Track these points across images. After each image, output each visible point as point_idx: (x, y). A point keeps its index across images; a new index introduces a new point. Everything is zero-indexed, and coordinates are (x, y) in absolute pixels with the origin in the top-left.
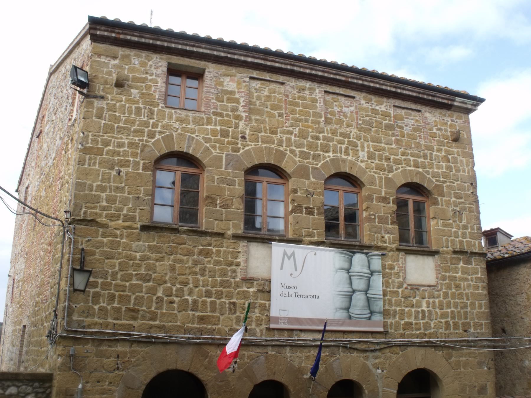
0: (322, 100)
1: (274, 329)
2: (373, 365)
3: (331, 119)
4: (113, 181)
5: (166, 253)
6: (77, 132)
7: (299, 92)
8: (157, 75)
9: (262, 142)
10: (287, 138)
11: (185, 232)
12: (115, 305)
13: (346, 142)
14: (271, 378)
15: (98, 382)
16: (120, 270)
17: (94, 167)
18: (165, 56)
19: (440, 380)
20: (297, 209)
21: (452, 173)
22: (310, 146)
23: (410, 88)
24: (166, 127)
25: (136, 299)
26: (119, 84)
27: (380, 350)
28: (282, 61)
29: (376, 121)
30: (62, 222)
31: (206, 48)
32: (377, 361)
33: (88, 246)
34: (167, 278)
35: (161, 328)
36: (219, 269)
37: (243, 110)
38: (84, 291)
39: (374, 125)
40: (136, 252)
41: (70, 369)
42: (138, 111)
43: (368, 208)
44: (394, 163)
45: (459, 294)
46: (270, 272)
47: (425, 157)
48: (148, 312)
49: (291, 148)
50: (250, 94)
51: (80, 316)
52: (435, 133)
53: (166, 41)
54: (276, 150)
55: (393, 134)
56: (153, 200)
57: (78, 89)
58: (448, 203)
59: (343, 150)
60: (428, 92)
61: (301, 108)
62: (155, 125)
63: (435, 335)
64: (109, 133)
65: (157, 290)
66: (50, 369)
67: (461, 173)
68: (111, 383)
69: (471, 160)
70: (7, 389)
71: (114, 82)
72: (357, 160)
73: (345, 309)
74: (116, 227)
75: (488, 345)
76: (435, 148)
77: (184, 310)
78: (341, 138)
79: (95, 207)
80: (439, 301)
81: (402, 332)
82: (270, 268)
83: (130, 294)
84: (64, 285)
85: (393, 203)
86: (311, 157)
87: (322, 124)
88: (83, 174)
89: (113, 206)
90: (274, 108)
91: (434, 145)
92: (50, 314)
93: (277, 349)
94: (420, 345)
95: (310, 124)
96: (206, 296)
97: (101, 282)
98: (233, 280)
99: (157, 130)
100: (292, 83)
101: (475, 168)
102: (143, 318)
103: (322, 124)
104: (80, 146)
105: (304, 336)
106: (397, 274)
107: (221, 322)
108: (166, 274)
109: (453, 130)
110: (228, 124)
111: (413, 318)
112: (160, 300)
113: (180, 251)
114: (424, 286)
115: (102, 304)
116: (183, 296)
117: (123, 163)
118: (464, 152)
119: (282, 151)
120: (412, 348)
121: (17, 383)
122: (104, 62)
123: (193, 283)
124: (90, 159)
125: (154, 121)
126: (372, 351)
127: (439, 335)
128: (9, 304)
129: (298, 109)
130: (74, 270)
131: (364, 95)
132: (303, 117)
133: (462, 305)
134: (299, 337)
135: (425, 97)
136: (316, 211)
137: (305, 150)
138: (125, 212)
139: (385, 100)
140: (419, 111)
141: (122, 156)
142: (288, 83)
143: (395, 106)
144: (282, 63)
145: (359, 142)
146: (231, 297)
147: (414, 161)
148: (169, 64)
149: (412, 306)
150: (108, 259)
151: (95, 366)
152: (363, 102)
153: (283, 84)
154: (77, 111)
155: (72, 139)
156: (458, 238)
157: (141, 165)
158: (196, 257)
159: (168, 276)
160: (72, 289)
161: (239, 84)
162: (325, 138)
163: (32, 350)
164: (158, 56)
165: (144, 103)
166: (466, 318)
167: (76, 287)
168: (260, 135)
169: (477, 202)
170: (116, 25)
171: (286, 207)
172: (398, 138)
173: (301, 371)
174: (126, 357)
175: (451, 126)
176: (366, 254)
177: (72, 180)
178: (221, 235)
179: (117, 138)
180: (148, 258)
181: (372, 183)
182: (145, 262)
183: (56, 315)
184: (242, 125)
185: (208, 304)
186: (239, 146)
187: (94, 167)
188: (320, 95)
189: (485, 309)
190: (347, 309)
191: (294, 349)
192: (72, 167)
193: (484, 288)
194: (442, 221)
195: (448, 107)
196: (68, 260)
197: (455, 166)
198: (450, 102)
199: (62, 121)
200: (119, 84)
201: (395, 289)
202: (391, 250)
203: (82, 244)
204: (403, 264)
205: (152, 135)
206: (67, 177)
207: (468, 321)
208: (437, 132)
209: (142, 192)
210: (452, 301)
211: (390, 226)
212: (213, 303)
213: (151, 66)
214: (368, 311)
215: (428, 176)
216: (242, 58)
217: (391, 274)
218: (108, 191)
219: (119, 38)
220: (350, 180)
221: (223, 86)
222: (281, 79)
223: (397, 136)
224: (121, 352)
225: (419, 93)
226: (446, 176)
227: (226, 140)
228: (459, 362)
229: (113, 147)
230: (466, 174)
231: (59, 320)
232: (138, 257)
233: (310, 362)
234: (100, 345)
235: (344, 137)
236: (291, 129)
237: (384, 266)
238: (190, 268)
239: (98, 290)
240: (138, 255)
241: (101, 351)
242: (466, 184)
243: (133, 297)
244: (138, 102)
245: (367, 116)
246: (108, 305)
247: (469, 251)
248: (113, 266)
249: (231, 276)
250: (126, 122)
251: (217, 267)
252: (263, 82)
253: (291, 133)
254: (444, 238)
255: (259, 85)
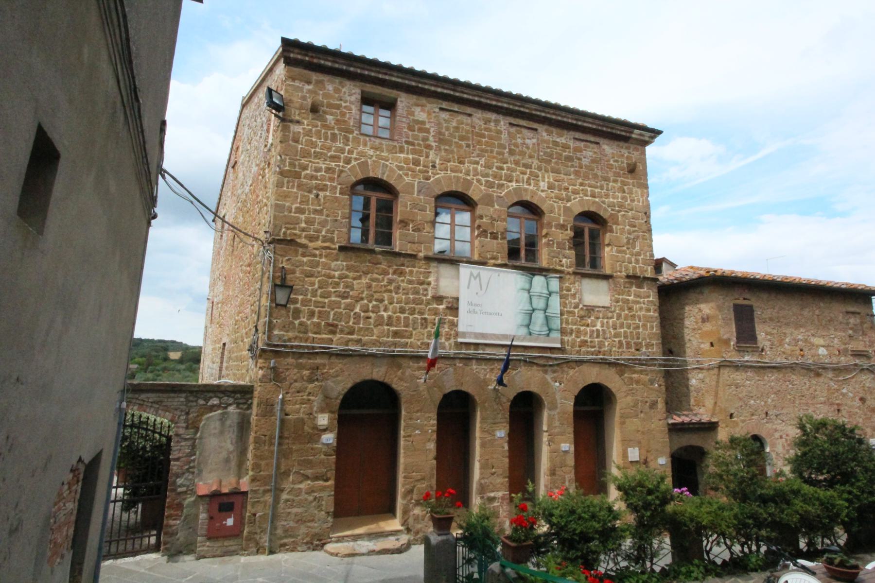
1: (461, 343)
6: (275, 158)
8: (351, 103)
12: (315, 320)
14: (458, 388)
16: (320, 288)
18: (358, 84)
20: (484, 233)
23: (590, 120)
24: (362, 154)
25: (334, 314)
26: (314, 109)
31: (398, 77)
35: (359, 341)
38: (285, 306)
41: (271, 381)
43: (547, 234)
46: (458, 291)
50: (439, 124)
51: (281, 330)
52: (612, 165)
54: (464, 179)
56: (350, 223)
62: (350, 152)
79: (294, 229)
81: (577, 349)
84: (265, 302)
87: (506, 155)
90: (462, 138)
91: (610, 175)
93: (464, 361)
98: (424, 298)
100: (479, 116)
101: (649, 199)
102: (342, 331)
103: (506, 155)
106: (574, 296)
114: (599, 307)
115: (302, 319)
128: (209, 325)
131: (545, 127)
135: (605, 129)
137: (490, 179)
138: (323, 233)
139: (565, 132)
140: (598, 143)
148: (363, 92)
149: (588, 325)
150: (308, 277)
152: (545, 134)
153: (470, 115)
155: (269, 164)
161: (429, 114)
164: (352, 83)
165: (339, 129)
167: (278, 302)
171: (472, 232)
175: (627, 158)
176: (545, 276)
177: (272, 201)
178: (413, 257)
180: (347, 277)
183: (257, 330)
186: (430, 174)
195: (626, 139)
196: (269, 278)
199: (257, 148)
200: (314, 109)
205: (348, 161)
206: (265, 200)
212: (406, 318)
213: (345, 93)
214: (547, 329)
216: (433, 88)
220: (532, 209)
222: (469, 110)
225: (599, 125)
232: (337, 276)
234: (300, 358)
235: (527, 168)
236: (477, 159)
237: (561, 289)
238: (385, 286)
240: (337, 274)
243: (332, 313)
244: (333, 128)
245: (548, 147)
246: (308, 319)
248: (313, 284)
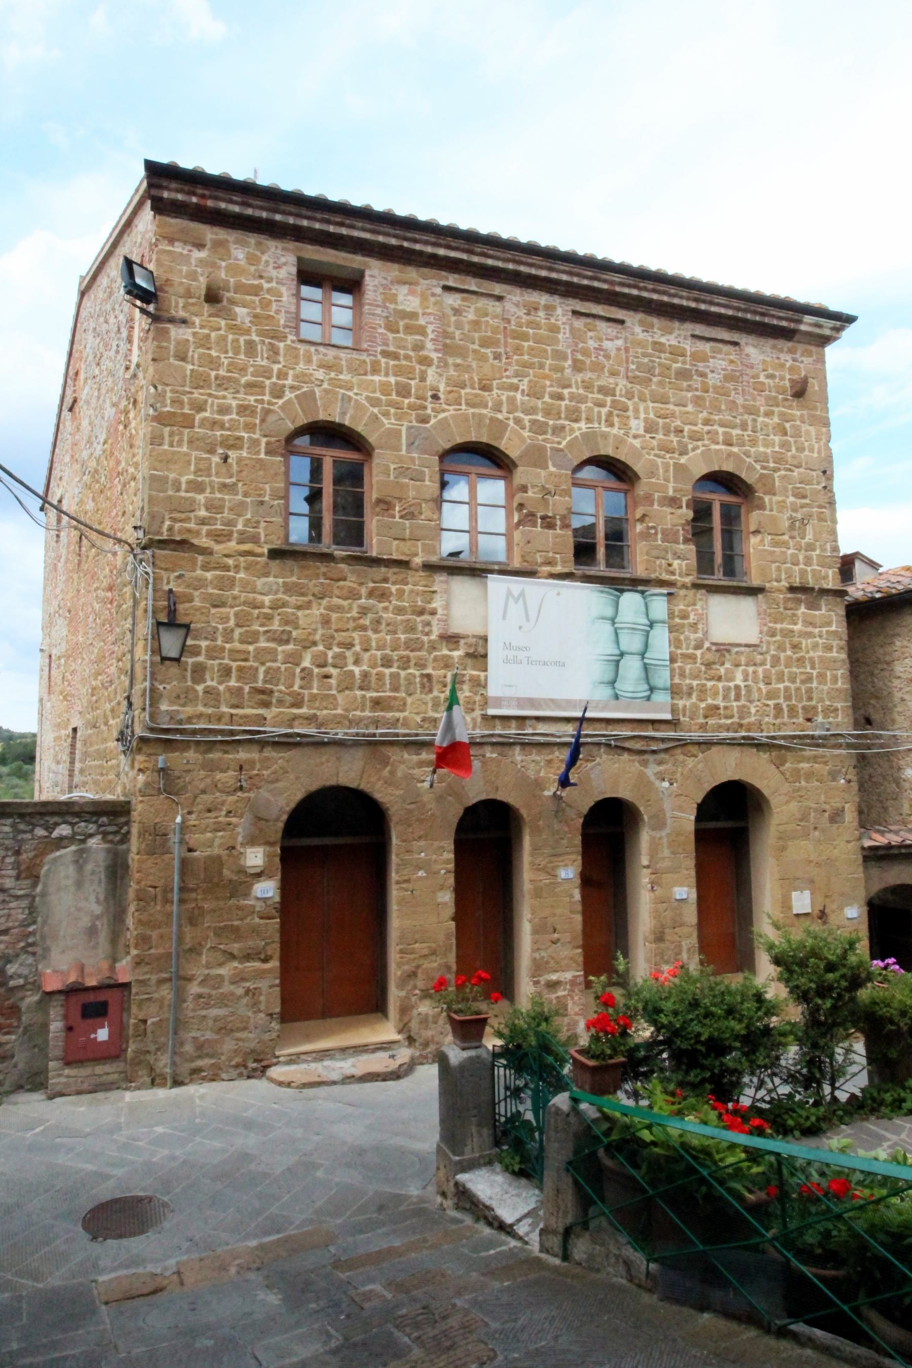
0: (567, 327)
1: (494, 717)
2: (655, 774)
3: (583, 362)
4: (217, 474)
5: (314, 595)
7: (528, 314)
9: (467, 404)
10: (508, 398)
11: (344, 560)
12: (233, 683)
13: (609, 404)
15: (209, 811)
17: (179, 449)
18: (292, 245)
19: (766, 801)
20: (529, 518)
21: (789, 454)
22: (547, 413)
24: (302, 378)
25: (267, 672)
26: (212, 297)
27: (666, 750)
28: (498, 254)
29: (660, 364)
30: (129, 545)
31: (364, 229)
32: (661, 768)
33: (179, 586)
34: (317, 637)
35: (311, 719)
36: (403, 621)
37: (433, 347)
38: (177, 660)
39: (657, 372)
40: (262, 594)
41: (160, 793)
42: (251, 347)
43: (644, 516)
44: (691, 438)
45: (798, 660)
47: (744, 426)
48: (288, 694)
49: (516, 414)
50: (442, 317)
51: (172, 703)
52: (762, 383)
53: (290, 214)
55: (689, 386)
57: (138, 303)
58: (782, 506)
59: (604, 418)
60: (754, 307)
61: (531, 343)
62: (282, 375)
63: (759, 726)
64: (202, 387)
65: (301, 656)
66: (124, 795)
67: (806, 453)
68: (230, 812)
69: (824, 430)
70: (54, 829)
71: (203, 292)
72: (626, 434)
73: (608, 683)
74: (226, 552)
75: (847, 744)
76: (762, 409)
77: (347, 688)
78: (600, 396)
79: (187, 520)
80: (765, 671)
82: (486, 619)
83: (256, 664)
84: (143, 654)
85: (687, 507)
86: (550, 431)
87: (568, 371)
88: (161, 461)
89: (219, 516)
90: (485, 343)
91: (761, 403)
92: (119, 703)
93: (499, 748)
94: (732, 743)
95: (547, 371)
96: (382, 666)
97: (207, 646)
98: (425, 638)
99: (286, 382)
100: (516, 297)
102: (280, 702)
103: (568, 371)
104: (151, 411)
105: (542, 728)
106: (694, 626)
107: (408, 707)
108: (315, 630)
109: (795, 377)
110: (407, 372)
111: (721, 698)
112: (307, 675)
113: (336, 592)
115: (209, 683)
116: (346, 665)
117: (231, 442)
118: (813, 416)
119: (501, 421)
120: (720, 747)
121: (70, 819)
122: (181, 254)
123: (361, 643)
124: (171, 434)
125: (280, 366)
126: (654, 752)
127: (764, 727)
129: (526, 344)
130: (159, 624)
131: (640, 316)
132: (536, 360)
133: (803, 677)
134: (534, 729)
135: (749, 316)
136: (558, 523)
138: (240, 527)
139: (677, 324)
140: (736, 344)
141: (229, 429)
142: (509, 297)
143: (693, 336)
144: (498, 258)
145: (630, 403)
146: (424, 666)
147: (725, 433)
148: (300, 260)
149: (719, 679)
150: (215, 606)
151: (202, 786)
152: (638, 329)
153: (500, 298)
154: (140, 348)
155: (135, 402)
156: (797, 564)
157: (263, 445)
158: (363, 601)
159: (320, 632)
160: (158, 658)
161: (424, 298)
162: (572, 397)
163: (91, 767)
164: (280, 244)
165: (260, 333)
166: (810, 699)
167: (164, 654)
168: (463, 392)
169: (832, 503)
170: (195, 179)
171: (509, 516)
172: (697, 393)
173: (539, 784)
174: (253, 768)
175: (791, 369)
176: (642, 592)
177: (144, 471)
178: (403, 564)
179: (217, 397)
180: (284, 605)
181: (652, 474)
182: (280, 610)
183: (130, 704)
184: (431, 373)
185: (387, 678)
186: (429, 411)
187: (179, 449)
188: (564, 319)
189: (843, 683)
190: (612, 683)
191: (527, 748)
192: (140, 451)
193: (842, 648)
194: (770, 537)
195: (787, 334)
196: (146, 611)
197: (795, 442)
198: (792, 325)
200: (212, 297)
201: (691, 651)
202: (684, 586)
203: (168, 583)
204: (703, 609)
205: (278, 393)
206: (131, 470)
207: (813, 703)
208: (766, 381)
209: (268, 492)
210: (786, 671)
211: (682, 546)
214: (646, 687)
215: (748, 460)
216: (429, 249)
217: (683, 626)
218: (208, 490)
219: (205, 206)
221: (396, 303)
223: (697, 390)
224: (246, 761)
225: (738, 309)
226: (779, 459)
227: (407, 401)
228: (798, 771)
229: (212, 413)
230: (816, 455)
231: (137, 713)
232: (267, 603)
233: (553, 770)
235: (606, 394)
236: (515, 381)
237: (671, 615)
238: (354, 619)
239: (201, 659)
240: (267, 600)
241: (212, 760)
242: (814, 473)
243: (262, 669)
244: (248, 332)
245: (645, 355)
246: (220, 683)
247: (817, 587)
248: (225, 619)
249: (422, 632)
250: (232, 367)
251: (399, 618)
252: (465, 295)
253: (515, 388)
254: (774, 566)
255: (459, 302)
